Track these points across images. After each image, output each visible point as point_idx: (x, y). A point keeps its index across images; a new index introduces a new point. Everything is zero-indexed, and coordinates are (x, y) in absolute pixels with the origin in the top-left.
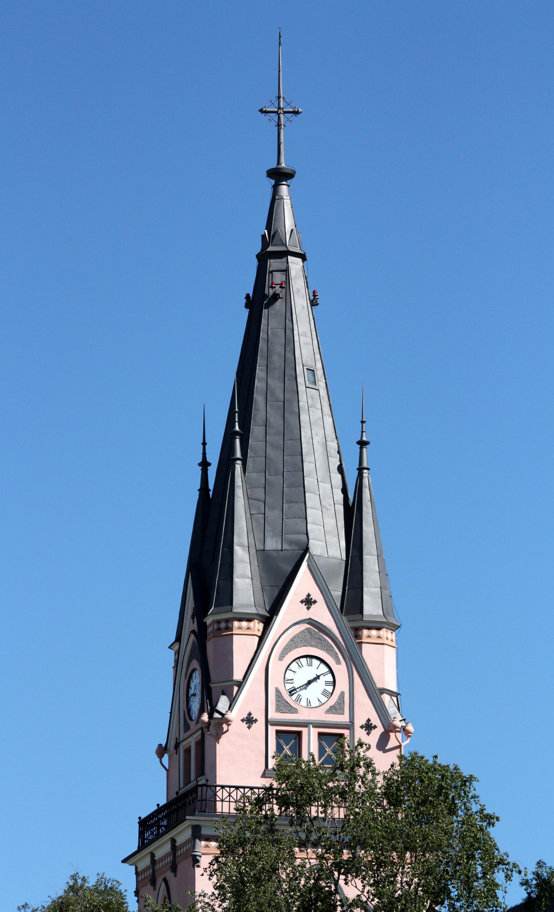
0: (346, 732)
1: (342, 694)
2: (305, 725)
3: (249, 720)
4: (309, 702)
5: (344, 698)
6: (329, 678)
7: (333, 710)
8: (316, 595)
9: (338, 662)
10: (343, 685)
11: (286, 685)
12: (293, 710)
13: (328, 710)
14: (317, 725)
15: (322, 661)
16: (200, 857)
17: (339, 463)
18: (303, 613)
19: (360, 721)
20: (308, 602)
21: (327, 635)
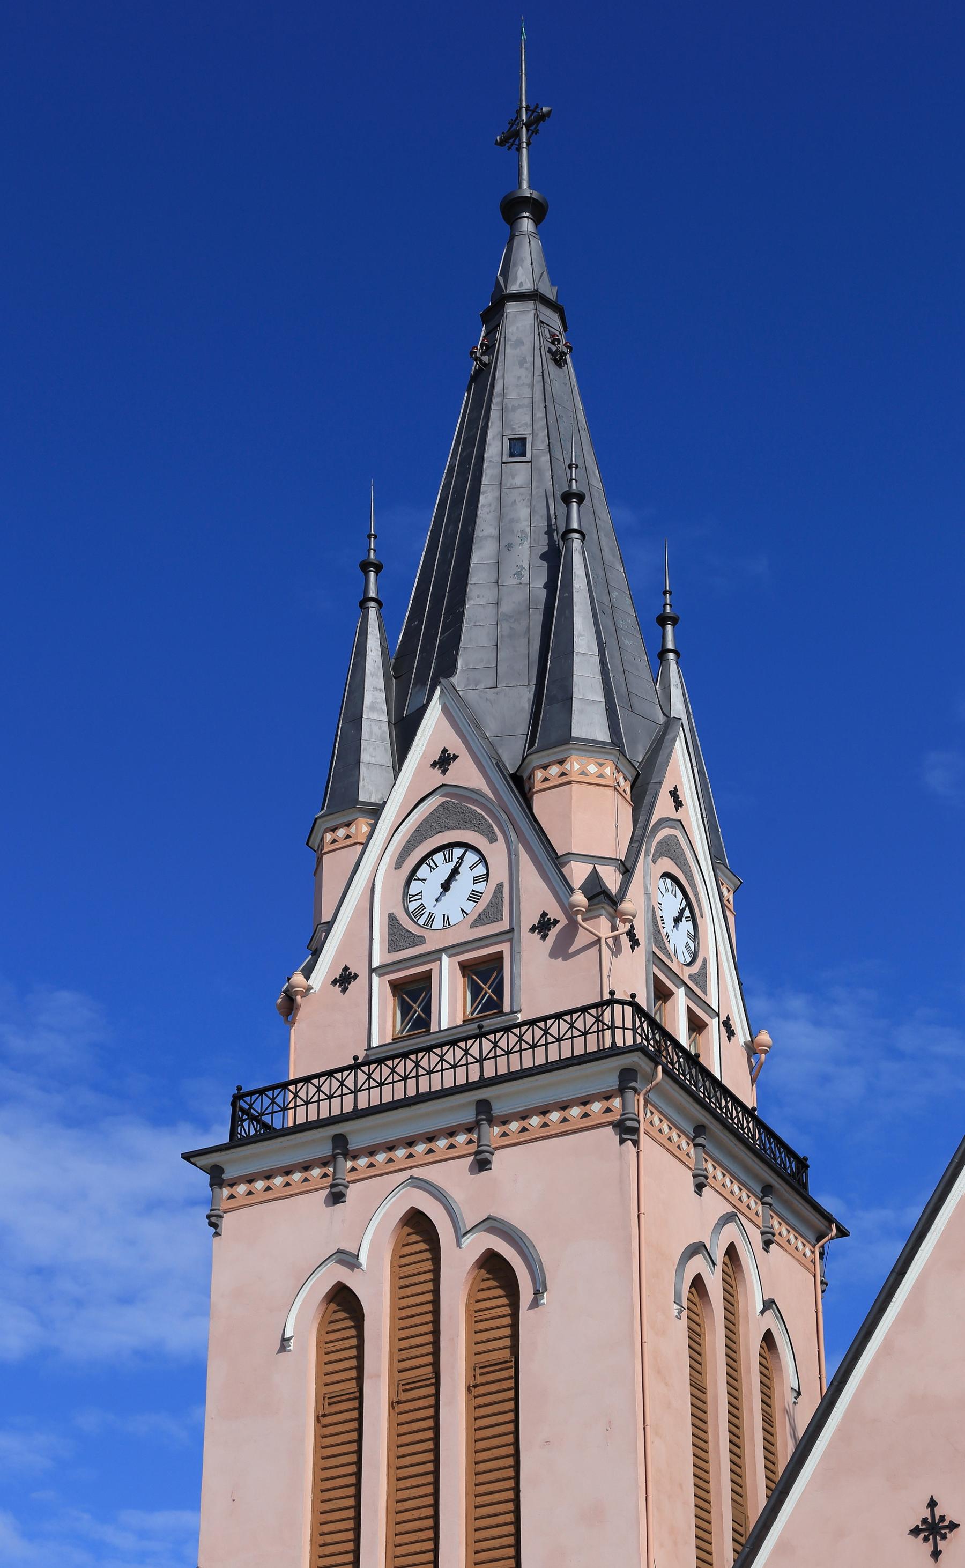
0: (505, 948)
1: (500, 886)
2: (435, 955)
3: (345, 979)
4: (446, 920)
5: (502, 893)
6: (471, 858)
7: (481, 920)
8: (455, 745)
9: (492, 839)
10: (499, 873)
11: (419, 922)
12: (421, 940)
13: (476, 920)
14: (451, 950)
15: (468, 847)
16: (221, 1217)
17: (812, 1193)
18: (437, 778)
19: (529, 918)
20: (444, 761)
21: (475, 802)
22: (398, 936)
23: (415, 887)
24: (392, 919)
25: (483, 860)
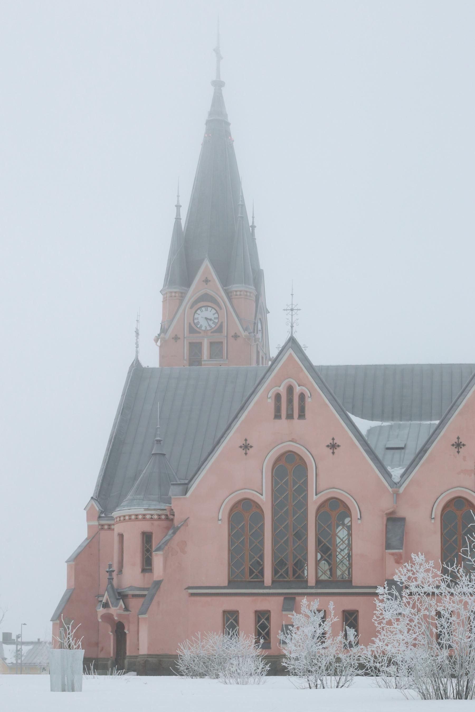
6: (214, 311)
20: (207, 281)
22: (192, 330)
23: (196, 316)
24: (190, 324)
25: (217, 312)
